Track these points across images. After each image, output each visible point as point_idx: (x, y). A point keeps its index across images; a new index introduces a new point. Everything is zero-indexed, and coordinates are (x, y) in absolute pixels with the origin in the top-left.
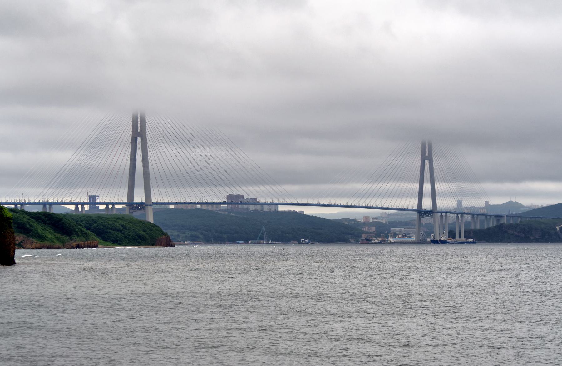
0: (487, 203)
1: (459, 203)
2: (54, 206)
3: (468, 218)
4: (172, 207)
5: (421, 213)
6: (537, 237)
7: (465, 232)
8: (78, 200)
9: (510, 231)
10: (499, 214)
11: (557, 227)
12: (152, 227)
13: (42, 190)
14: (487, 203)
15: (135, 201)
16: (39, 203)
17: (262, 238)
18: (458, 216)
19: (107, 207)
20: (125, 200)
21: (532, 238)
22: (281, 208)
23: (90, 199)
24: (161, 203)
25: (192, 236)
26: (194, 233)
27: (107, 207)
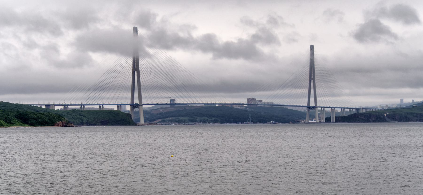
0: (413, 100)
1: (402, 100)
2: (122, 106)
3: (354, 110)
4: (217, 105)
5: (310, 108)
6: (374, 119)
7: (336, 117)
8: (99, 103)
9: (360, 117)
10: (358, 107)
11: (385, 115)
12: (128, 115)
13: (88, 94)
14: (413, 100)
15: (135, 103)
16: (79, 105)
17: (249, 121)
18: (342, 110)
19: (322, 109)
20: (129, 102)
21: (371, 120)
22: (289, 108)
23: (170, 102)
24: (210, 104)
25: (215, 120)
26: (216, 118)
27: (322, 109)
